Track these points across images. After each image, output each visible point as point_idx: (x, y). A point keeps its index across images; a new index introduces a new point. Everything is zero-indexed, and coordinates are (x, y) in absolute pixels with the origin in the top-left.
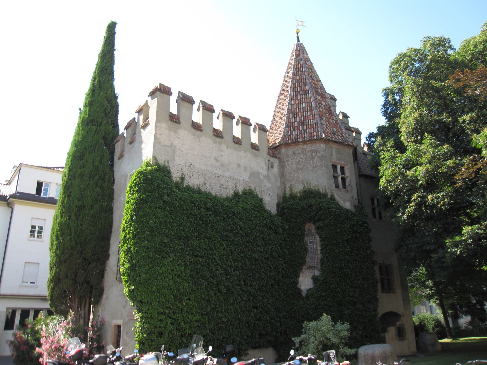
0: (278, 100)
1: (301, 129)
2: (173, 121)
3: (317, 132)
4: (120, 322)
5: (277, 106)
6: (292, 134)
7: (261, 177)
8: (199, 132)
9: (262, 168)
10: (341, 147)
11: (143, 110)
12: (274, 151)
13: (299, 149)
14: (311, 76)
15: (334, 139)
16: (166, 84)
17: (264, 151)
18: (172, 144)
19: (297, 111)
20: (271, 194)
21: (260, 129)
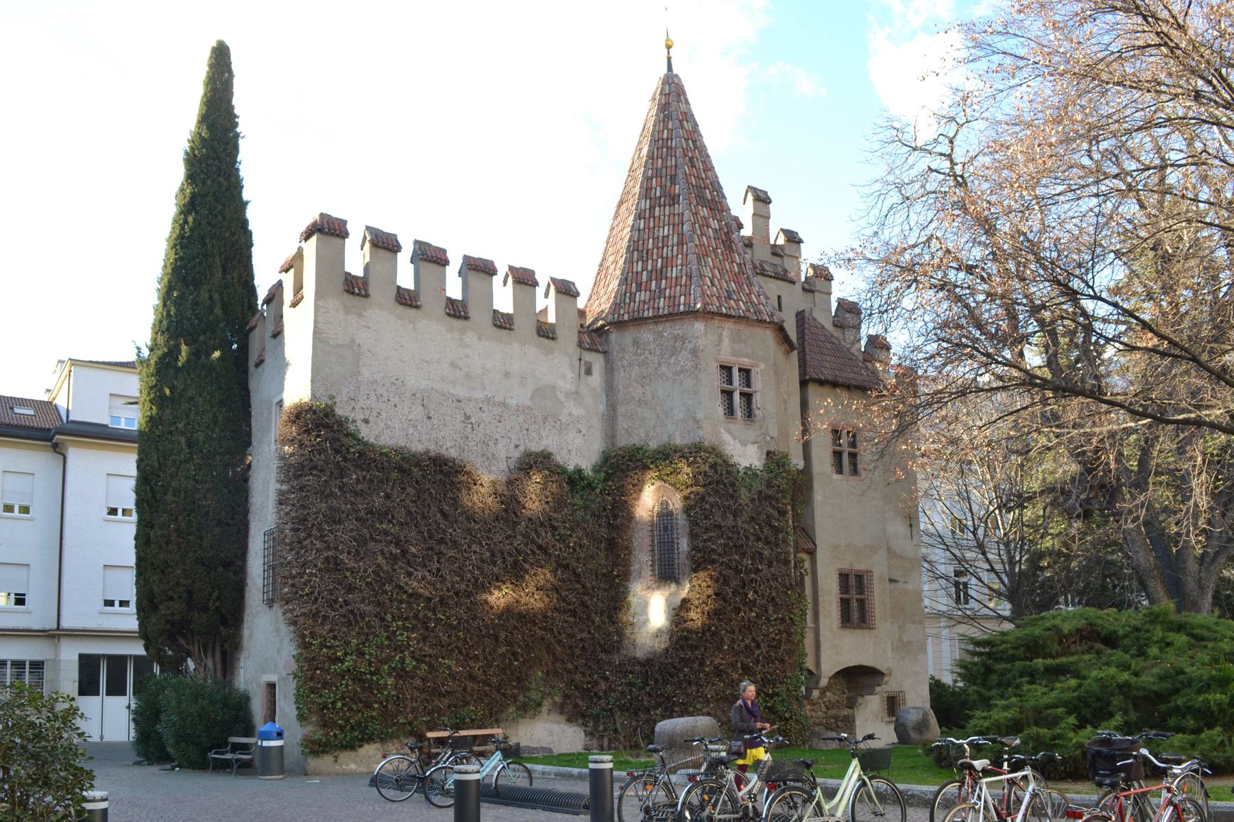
0: (615, 217)
1: (653, 287)
2: (353, 293)
3: (687, 294)
4: (273, 678)
5: (612, 229)
6: (633, 299)
7: (561, 396)
8: (413, 311)
9: (564, 376)
10: (742, 328)
11: (294, 264)
12: (595, 337)
13: (646, 334)
14: (691, 159)
15: (724, 311)
16: (336, 213)
17: (568, 337)
18: (353, 341)
19: (650, 246)
20: (584, 431)
21: (558, 291)
